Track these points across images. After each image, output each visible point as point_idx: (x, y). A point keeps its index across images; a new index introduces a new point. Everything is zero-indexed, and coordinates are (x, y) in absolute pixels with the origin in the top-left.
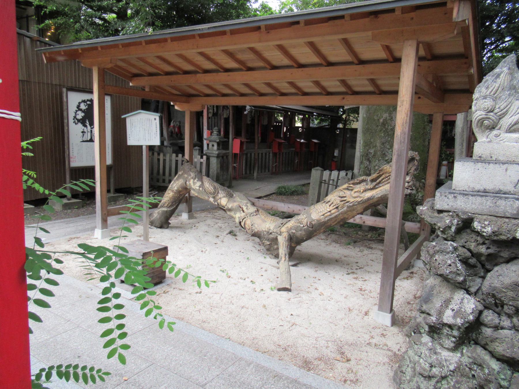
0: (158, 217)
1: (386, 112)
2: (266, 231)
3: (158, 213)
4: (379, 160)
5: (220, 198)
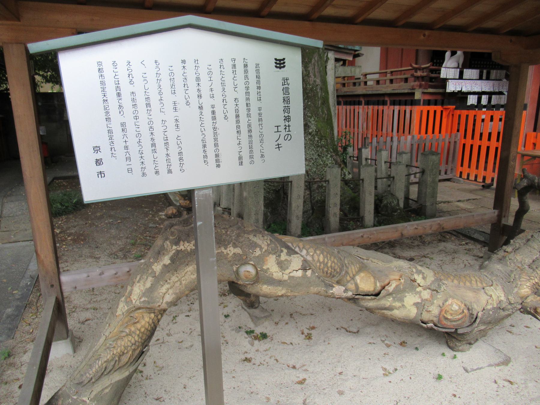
5: (353, 278)
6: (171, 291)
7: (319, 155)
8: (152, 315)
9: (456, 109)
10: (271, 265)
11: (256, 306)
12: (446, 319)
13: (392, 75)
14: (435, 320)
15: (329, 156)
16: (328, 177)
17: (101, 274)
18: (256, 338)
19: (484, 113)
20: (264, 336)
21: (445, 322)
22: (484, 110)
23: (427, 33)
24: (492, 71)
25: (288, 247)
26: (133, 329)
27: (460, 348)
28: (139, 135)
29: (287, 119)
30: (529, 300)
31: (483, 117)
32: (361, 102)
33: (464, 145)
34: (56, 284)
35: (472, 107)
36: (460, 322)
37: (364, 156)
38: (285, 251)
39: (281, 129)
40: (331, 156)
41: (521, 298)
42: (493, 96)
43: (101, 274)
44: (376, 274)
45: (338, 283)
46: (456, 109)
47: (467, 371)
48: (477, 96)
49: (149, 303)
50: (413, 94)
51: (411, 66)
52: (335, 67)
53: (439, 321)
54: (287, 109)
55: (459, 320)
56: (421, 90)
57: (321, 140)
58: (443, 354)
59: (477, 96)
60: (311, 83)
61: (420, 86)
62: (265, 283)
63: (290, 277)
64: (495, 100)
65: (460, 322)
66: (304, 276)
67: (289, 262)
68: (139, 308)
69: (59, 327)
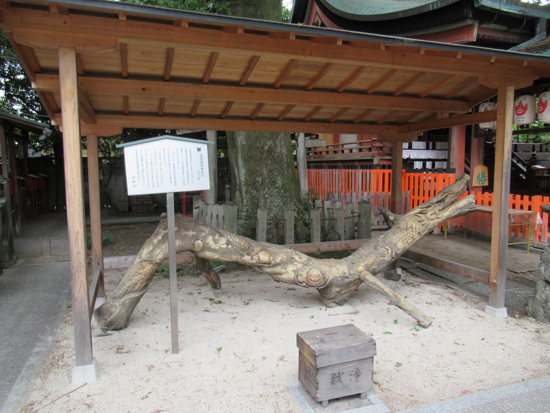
0: (124, 311)
1: (270, 140)
2: (340, 276)
3: (123, 305)
4: (269, 188)
5: (257, 254)
6: (161, 253)
7: (284, 203)
8: (152, 265)
9: (406, 172)
10: (210, 240)
11: (219, 287)
12: (311, 280)
13: (361, 145)
14: (305, 280)
15: (292, 204)
16: (286, 217)
17: (126, 260)
18: (216, 303)
19: (430, 175)
20: (220, 302)
21: (311, 282)
22: (430, 173)
23: (326, 125)
24: (437, 143)
25: (220, 233)
26: (142, 271)
27: (330, 305)
28: (148, 173)
29: (202, 169)
30: (362, 273)
31: (430, 178)
32: (357, 166)
33: (413, 200)
34: (101, 263)
35: (417, 170)
36: (319, 282)
37: (326, 207)
38: (218, 235)
39: (200, 172)
40: (294, 205)
41: (358, 272)
42: (436, 163)
43: (126, 260)
44: (270, 254)
45: (248, 254)
46: (406, 172)
47: (329, 315)
48: (421, 162)
49: (150, 258)
50: (372, 160)
51: (371, 139)
52: (305, 140)
53: (307, 281)
54: (202, 165)
55: (318, 280)
56: (379, 157)
57: (286, 192)
58: (321, 309)
59: (421, 162)
60: (278, 152)
61: (379, 154)
62: (208, 251)
63: (220, 248)
64: (437, 165)
65: (319, 282)
66: (227, 248)
67: (220, 240)
68: (145, 261)
69: (100, 289)
